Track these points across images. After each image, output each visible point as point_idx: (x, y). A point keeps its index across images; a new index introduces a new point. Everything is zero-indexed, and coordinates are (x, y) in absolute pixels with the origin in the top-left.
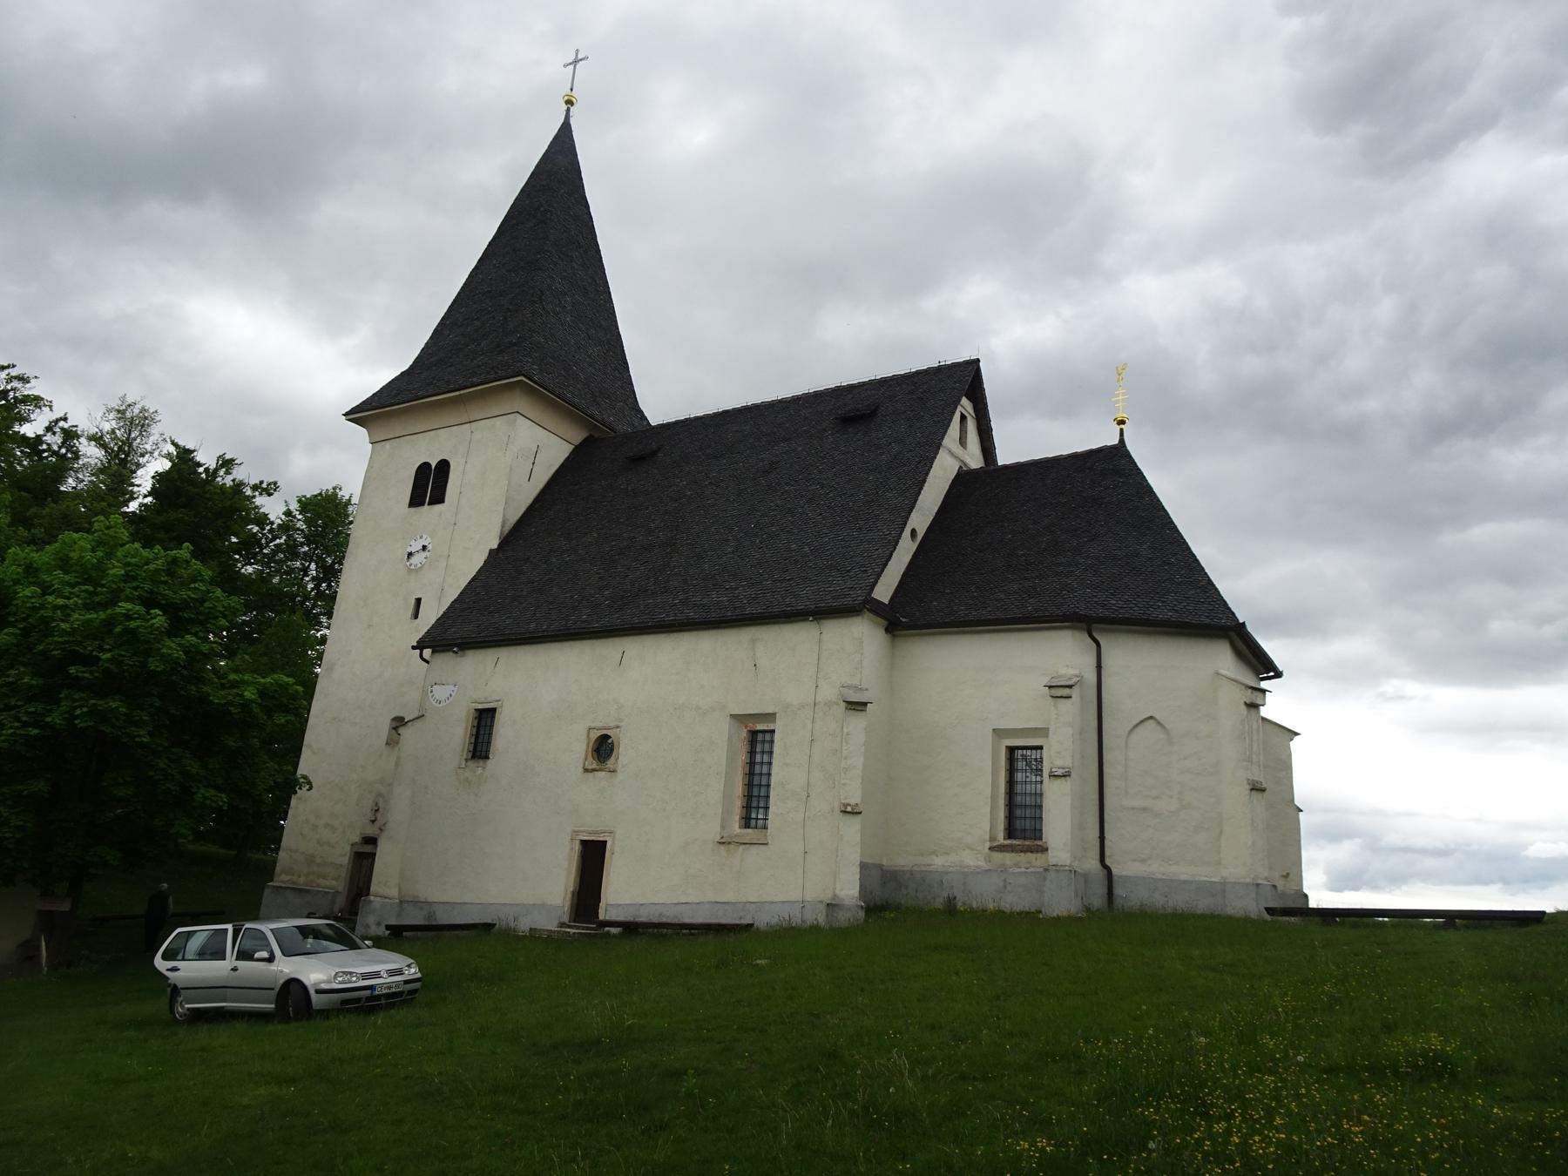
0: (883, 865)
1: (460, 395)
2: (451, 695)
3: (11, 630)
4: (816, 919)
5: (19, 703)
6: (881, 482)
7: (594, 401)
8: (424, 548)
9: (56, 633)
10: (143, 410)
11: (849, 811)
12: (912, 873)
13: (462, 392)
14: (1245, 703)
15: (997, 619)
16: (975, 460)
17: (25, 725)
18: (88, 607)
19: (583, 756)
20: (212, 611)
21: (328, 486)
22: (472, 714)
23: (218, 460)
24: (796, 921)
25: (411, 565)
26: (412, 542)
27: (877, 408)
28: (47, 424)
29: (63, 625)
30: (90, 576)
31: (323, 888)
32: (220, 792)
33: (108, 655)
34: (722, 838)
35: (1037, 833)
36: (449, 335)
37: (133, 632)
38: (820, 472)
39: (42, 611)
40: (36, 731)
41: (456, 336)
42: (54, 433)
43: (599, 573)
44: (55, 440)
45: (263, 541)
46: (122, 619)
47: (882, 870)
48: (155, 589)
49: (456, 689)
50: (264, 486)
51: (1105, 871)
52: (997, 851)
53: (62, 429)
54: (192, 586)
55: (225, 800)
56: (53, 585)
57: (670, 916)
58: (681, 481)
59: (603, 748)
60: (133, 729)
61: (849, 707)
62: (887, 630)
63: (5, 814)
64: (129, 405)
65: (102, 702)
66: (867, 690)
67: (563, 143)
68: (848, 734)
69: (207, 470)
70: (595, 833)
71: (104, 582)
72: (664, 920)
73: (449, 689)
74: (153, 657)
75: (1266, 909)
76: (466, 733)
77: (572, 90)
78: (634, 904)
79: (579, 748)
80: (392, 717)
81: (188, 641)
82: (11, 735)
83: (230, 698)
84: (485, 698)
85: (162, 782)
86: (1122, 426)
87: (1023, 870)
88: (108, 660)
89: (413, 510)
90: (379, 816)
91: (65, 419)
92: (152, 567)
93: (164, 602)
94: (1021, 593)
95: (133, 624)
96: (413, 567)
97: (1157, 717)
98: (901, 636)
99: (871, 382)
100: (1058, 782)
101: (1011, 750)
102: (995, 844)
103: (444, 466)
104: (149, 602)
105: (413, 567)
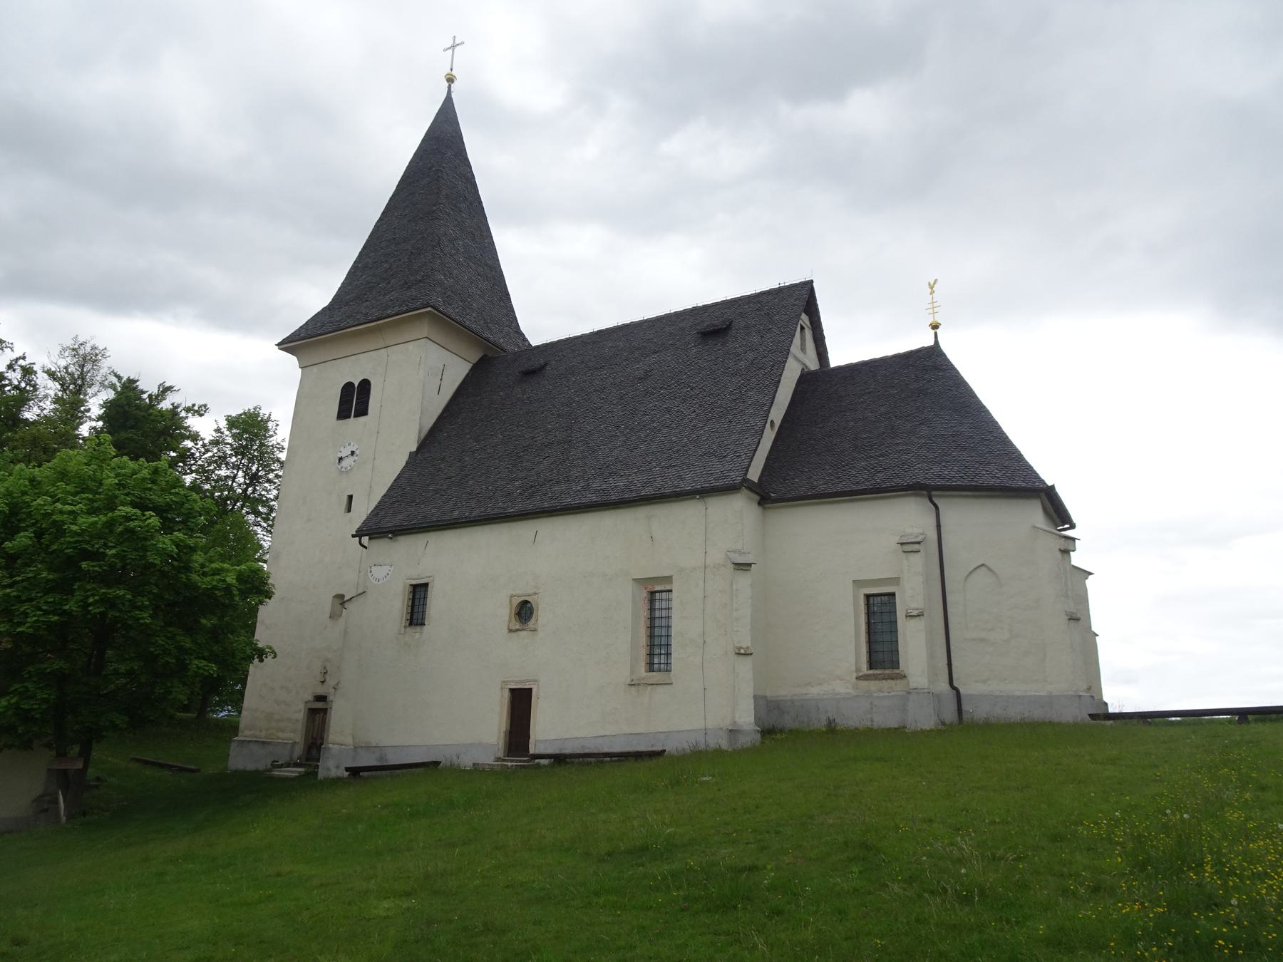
0: (766, 697)
1: (385, 323)
2: (388, 574)
3: (26, 533)
4: (718, 743)
5: (39, 595)
6: (743, 384)
7: (487, 326)
8: (353, 453)
9: (67, 535)
10: (94, 348)
11: (742, 653)
12: (792, 701)
13: (379, 322)
14: (1060, 550)
15: (851, 491)
16: (813, 365)
17: (46, 613)
18: (92, 511)
19: (507, 619)
20: (191, 511)
21: (249, 406)
22: (408, 589)
23: (159, 388)
24: (702, 747)
25: (342, 468)
26: (342, 449)
27: (730, 324)
28: (8, 363)
29: (74, 528)
30: (84, 485)
31: (283, 740)
32: (210, 663)
33: (114, 551)
34: (632, 680)
35: (895, 664)
36: (361, 276)
37: (131, 531)
38: (689, 377)
39: (54, 517)
40: (56, 618)
41: (368, 277)
42: (14, 370)
43: (508, 468)
44: (15, 376)
45: (198, 454)
46: (122, 520)
47: (767, 700)
48: (143, 495)
49: (392, 569)
50: (196, 408)
51: (955, 692)
52: (863, 680)
53: (22, 367)
54: (173, 491)
55: (215, 669)
56: (56, 495)
57: (592, 747)
58: (569, 389)
59: (524, 612)
60: (137, 613)
61: (737, 567)
62: (759, 504)
63: (32, 689)
64: (81, 344)
65: (109, 591)
66: (749, 553)
67: (446, 120)
68: (737, 590)
69: (150, 396)
70: (521, 682)
71: (101, 490)
72: (587, 751)
73: (385, 569)
74: (151, 551)
75: (1090, 715)
76: (403, 605)
77: (451, 70)
78: (561, 739)
79: (504, 613)
80: (333, 595)
81: (177, 537)
82: (36, 622)
83: (215, 583)
84: (417, 576)
85: (161, 656)
86: (936, 330)
87: (886, 694)
88: (114, 556)
89: (340, 422)
90: (328, 677)
91: (24, 358)
92: (139, 476)
93: (151, 505)
94: (870, 469)
95: (132, 524)
96: (343, 469)
97: (987, 563)
98: (769, 508)
99: (723, 303)
100: (913, 622)
101: (868, 597)
102: (860, 674)
103: (365, 385)
104: (142, 505)
105: (343, 469)
